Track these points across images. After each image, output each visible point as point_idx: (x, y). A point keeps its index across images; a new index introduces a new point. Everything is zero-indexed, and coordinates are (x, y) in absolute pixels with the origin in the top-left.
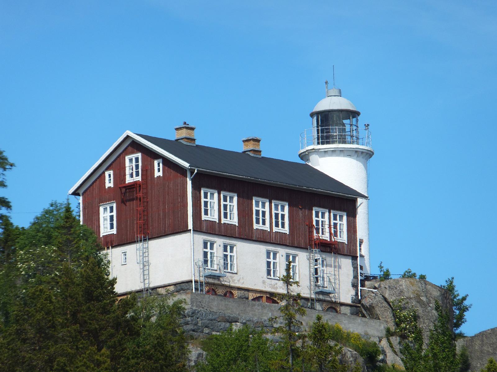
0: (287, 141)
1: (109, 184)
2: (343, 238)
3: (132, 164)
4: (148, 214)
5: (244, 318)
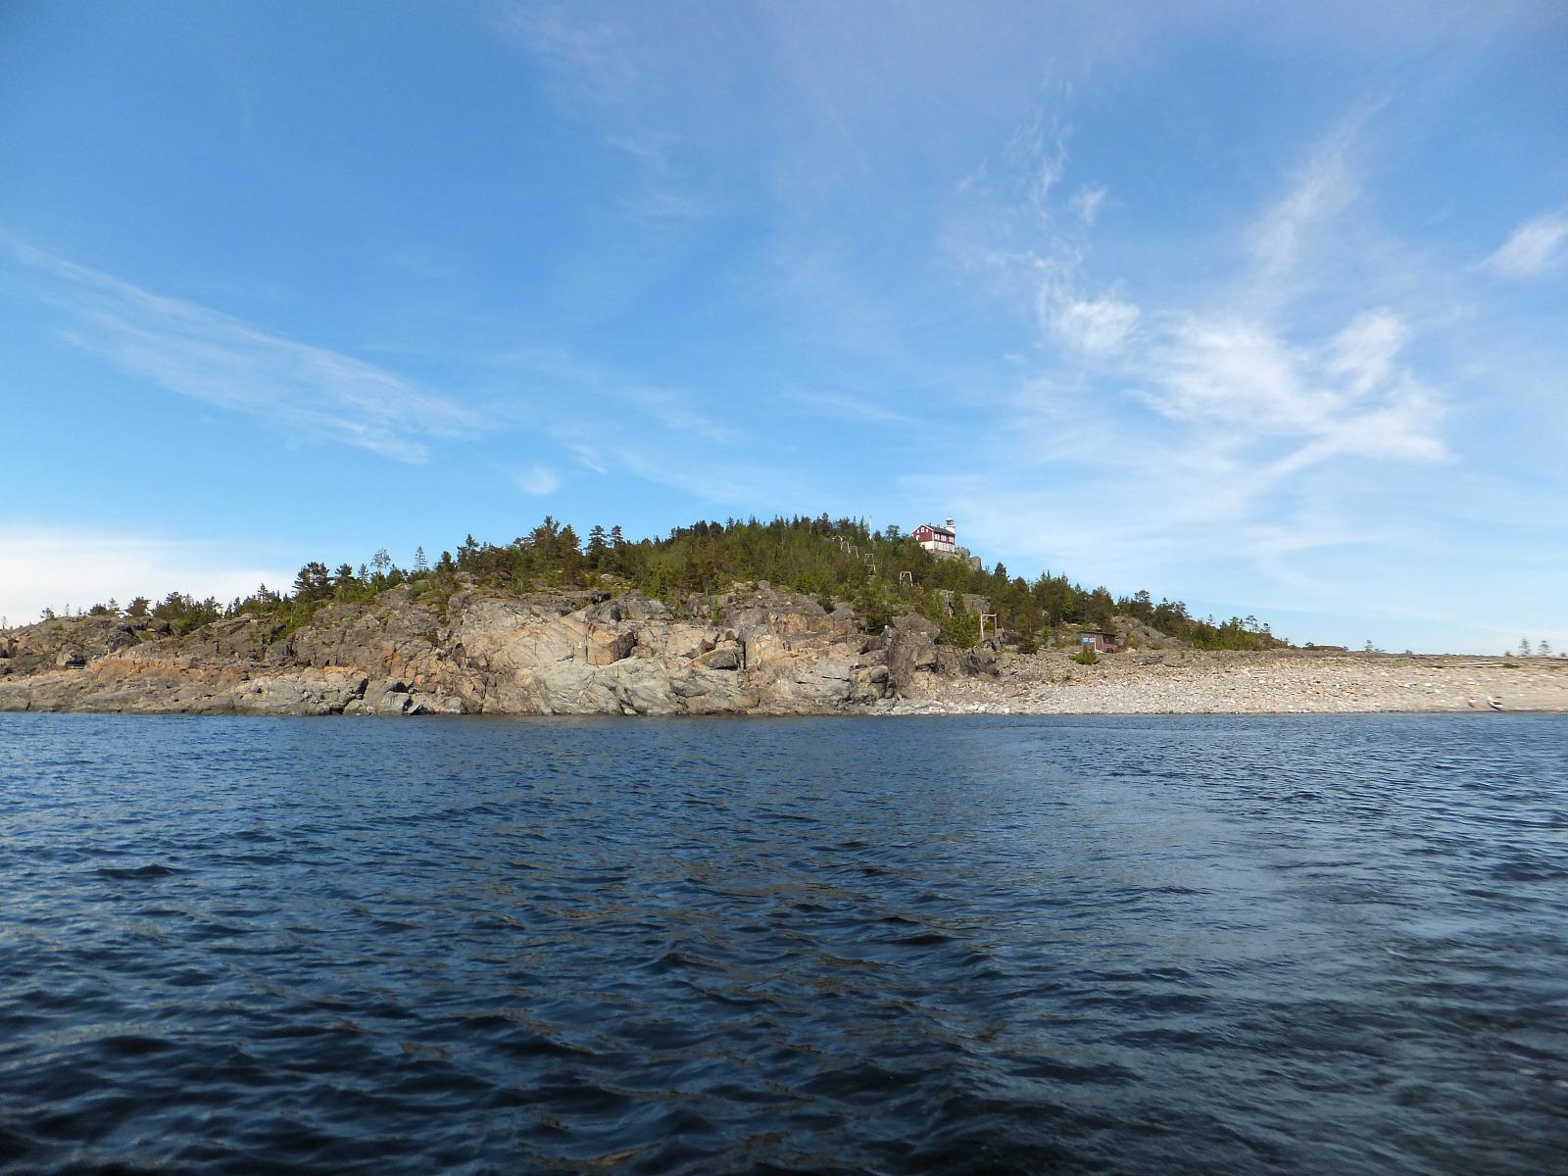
4: (926, 537)
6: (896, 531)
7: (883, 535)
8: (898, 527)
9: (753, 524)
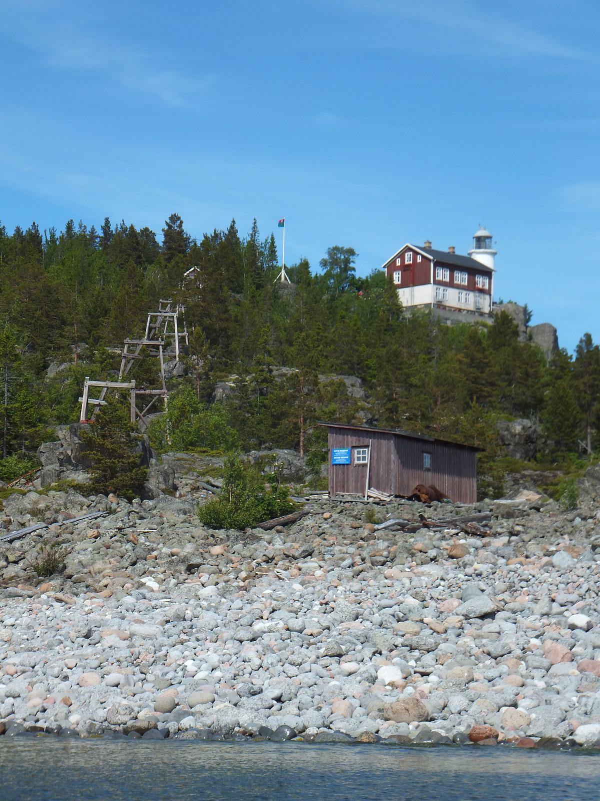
0: (465, 249)
1: (398, 263)
2: (487, 287)
3: (408, 256)
4: (415, 275)
5: (451, 318)
6: (347, 261)
7: (316, 270)
8: (351, 252)
9: (175, 233)
